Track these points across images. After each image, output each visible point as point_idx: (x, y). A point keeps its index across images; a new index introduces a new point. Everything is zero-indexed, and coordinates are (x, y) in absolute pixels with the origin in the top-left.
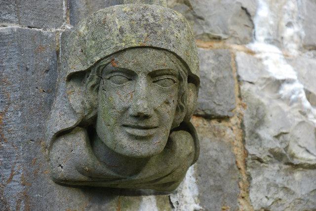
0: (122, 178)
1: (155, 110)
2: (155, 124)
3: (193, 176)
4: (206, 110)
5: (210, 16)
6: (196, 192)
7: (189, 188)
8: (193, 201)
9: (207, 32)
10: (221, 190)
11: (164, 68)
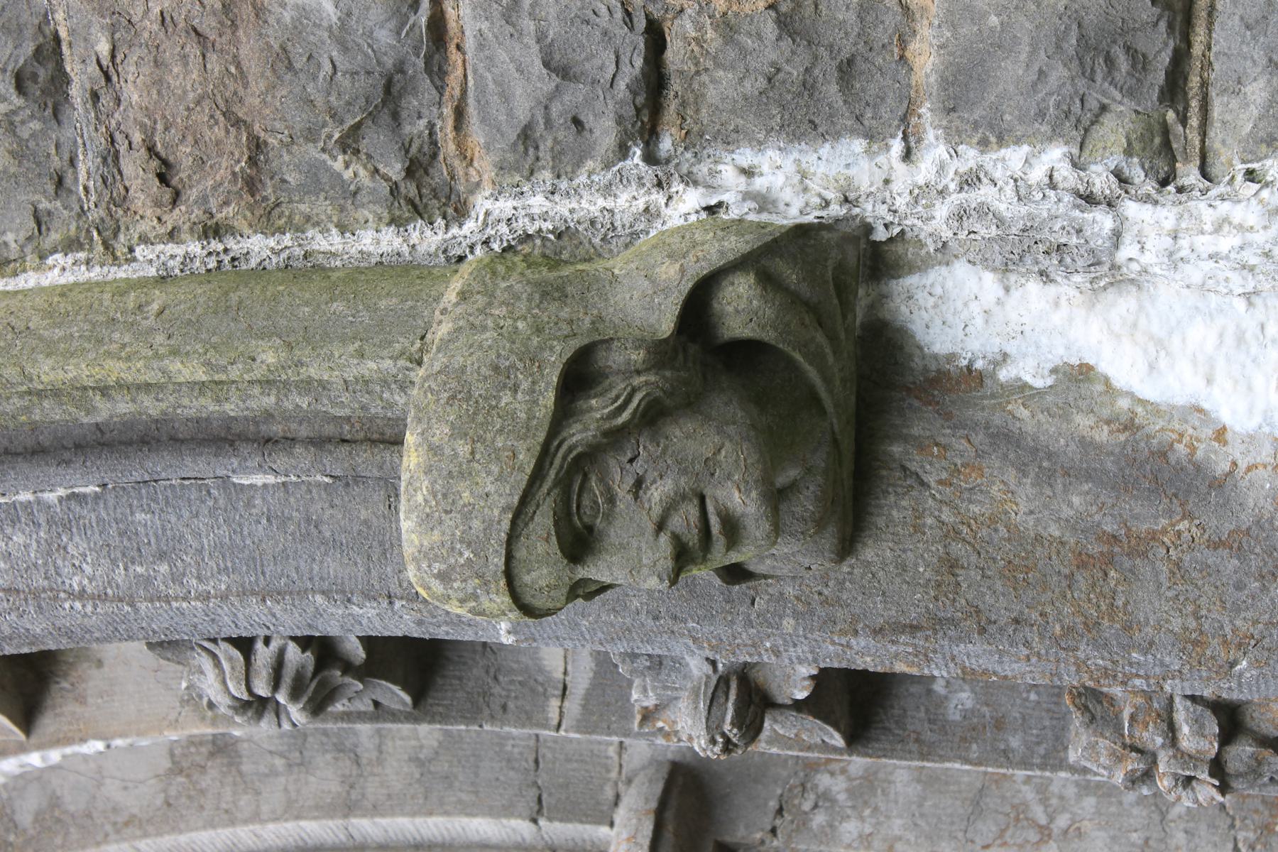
0: (833, 433)
1: (660, 527)
2: (693, 511)
3: (816, 151)
4: (635, 107)
5: (379, 63)
6: (859, 145)
7: (848, 166)
8: (881, 159)
9: (421, 63)
10: (850, 62)
11: (554, 539)
